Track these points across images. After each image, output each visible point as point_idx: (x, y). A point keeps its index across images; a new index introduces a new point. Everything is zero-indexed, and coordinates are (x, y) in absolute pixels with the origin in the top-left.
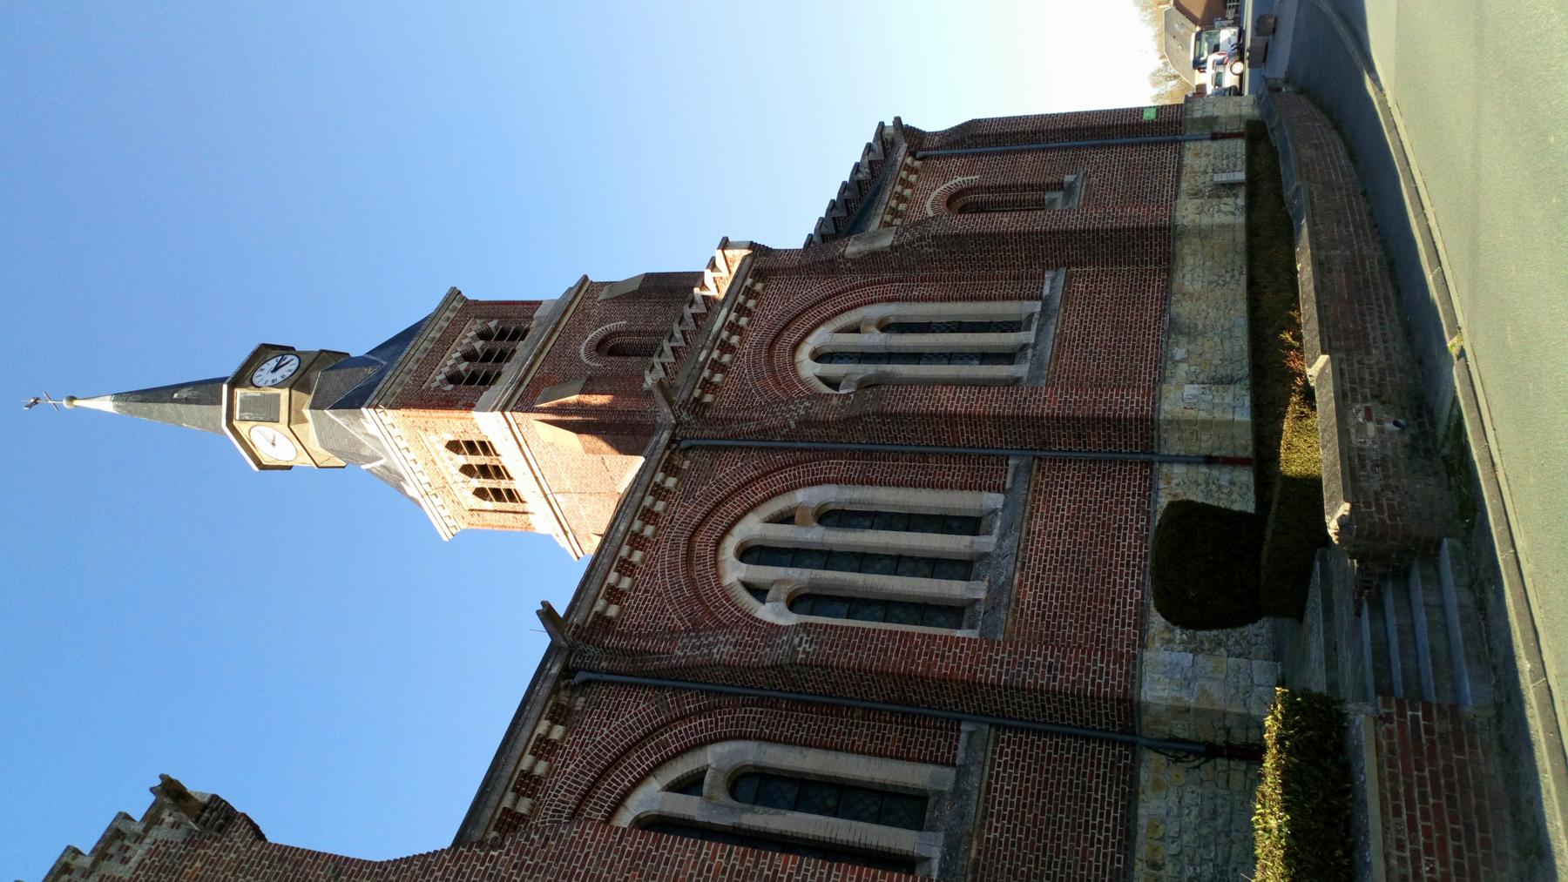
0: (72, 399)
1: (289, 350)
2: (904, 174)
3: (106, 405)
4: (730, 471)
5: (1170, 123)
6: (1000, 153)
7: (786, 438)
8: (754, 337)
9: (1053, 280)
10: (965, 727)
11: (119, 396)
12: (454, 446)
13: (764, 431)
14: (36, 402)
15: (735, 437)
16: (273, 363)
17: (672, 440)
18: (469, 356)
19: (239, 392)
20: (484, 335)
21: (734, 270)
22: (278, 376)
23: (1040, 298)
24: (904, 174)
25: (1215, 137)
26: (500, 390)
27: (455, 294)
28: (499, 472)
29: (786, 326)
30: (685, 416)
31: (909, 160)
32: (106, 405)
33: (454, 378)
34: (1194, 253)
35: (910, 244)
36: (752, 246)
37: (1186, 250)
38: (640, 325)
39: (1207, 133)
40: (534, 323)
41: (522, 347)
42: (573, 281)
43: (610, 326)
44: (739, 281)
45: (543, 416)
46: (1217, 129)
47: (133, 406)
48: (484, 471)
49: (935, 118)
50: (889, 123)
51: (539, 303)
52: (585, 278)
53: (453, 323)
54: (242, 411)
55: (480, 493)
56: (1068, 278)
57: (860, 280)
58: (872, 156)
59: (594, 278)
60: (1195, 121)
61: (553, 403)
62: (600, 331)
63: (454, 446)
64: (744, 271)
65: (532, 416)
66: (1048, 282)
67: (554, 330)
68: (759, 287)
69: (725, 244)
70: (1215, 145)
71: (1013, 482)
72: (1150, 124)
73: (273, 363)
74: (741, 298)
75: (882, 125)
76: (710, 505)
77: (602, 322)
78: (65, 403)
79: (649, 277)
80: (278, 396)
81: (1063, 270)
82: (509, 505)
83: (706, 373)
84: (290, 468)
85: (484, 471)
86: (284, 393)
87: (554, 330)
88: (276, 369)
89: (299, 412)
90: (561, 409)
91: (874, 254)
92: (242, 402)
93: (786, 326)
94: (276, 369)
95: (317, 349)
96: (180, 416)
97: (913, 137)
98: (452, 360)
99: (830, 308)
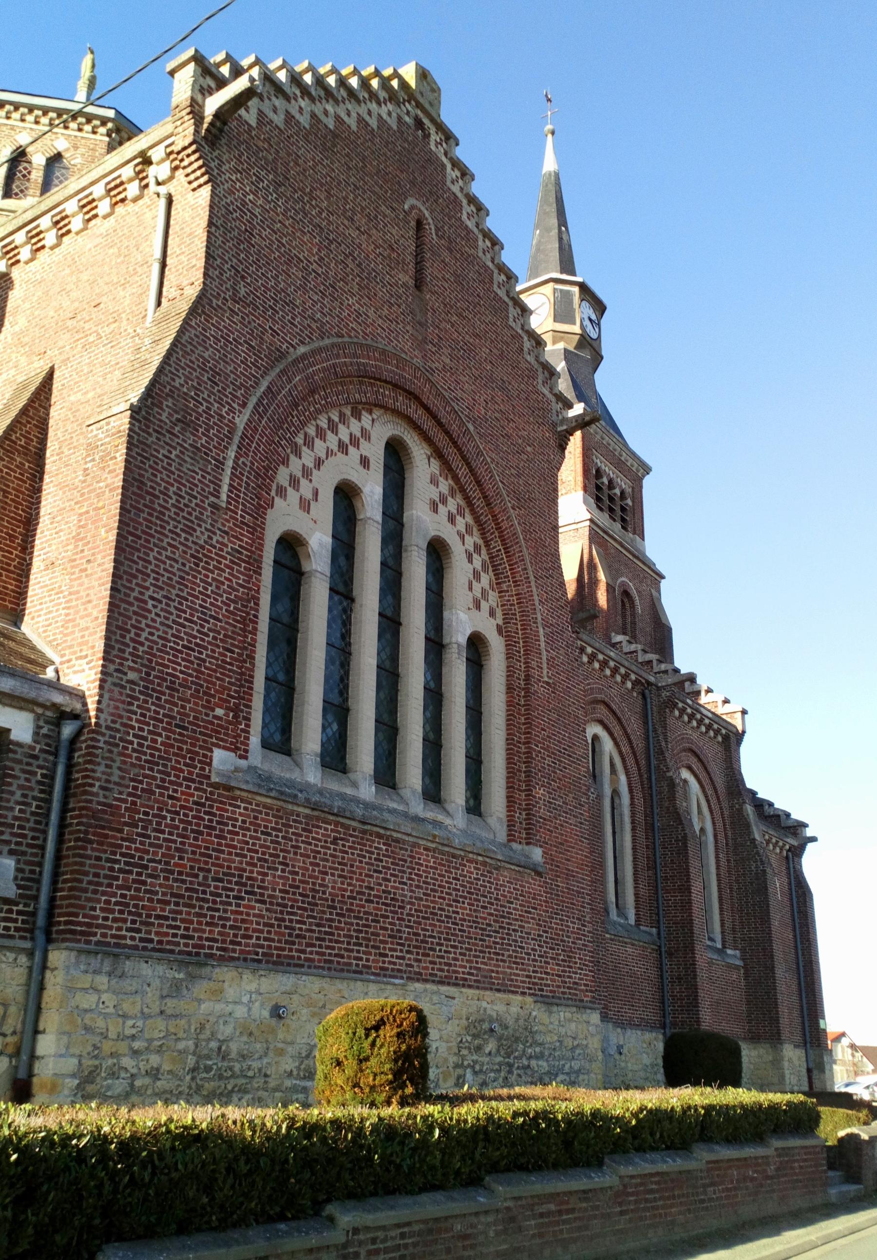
0: (553, 133)
2: (781, 844)
3: (550, 164)
4: (634, 726)
5: (818, 1039)
6: (793, 915)
7: (658, 767)
8: (695, 736)
9: (735, 956)
10: (654, 930)
11: (557, 175)
13: (662, 753)
14: (549, 100)
15: (655, 730)
16: (594, 317)
17: (649, 683)
18: (611, 485)
19: (576, 290)
21: (724, 717)
22: (587, 323)
23: (724, 947)
24: (781, 844)
25: (809, 1071)
26: (604, 519)
27: (647, 470)
29: (700, 760)
30: (665, 694)
31: (787, 847)
32: (550, 164)
33: (599, 474)
34: (760, 1057)
35: (758, 853)
36: (744, 732)
37: (762, 1051)
38: (639, 625)
39: (811, 1065)
40: (631, 535)
41: (618, 526)
42: (660, 567)
43: (637, 601)
44: (724, 724)
45: (586, 552)
46: (815, 1072)
47: (552, 188)
49: (812, 864)
50: (809, 832)
51: (643, 538)
52: (663, 577)
53: (630, 470)
54: (561, 291)
56: (737, 967)
57: (726, 813)
58: (783, 817)
60: (822, 1057)
61: (597, 560)
62: (634, 593)
64: (730, 728)
65: (587, 542)
66: (648, 929)
67: (634, 556)
68: (720, 739)
69: (744, 712)
70: (804, 1071)
71: (646, 932)
72: (818, 1024)
73: (594, 317)
74: (716, 726)
75: (805, 825)
76: (619, 714)
77: (638, 592)
78: (549, 127)
79: (670, 630)
80: (574, 324)
81: (739, 963)
83: (680, 705)
86: (577, 329)
87: (634, 556)
88: (590, 320)
89: (562, 339)
90: (592, 566)
91: (748, 826)
92: (568, 292)
93: (700, 760)
94: (590, 320)
95: (603, 353)
96: (548, 230)
97: (798, 851)
98: (609, 470)
99: (710, 792)
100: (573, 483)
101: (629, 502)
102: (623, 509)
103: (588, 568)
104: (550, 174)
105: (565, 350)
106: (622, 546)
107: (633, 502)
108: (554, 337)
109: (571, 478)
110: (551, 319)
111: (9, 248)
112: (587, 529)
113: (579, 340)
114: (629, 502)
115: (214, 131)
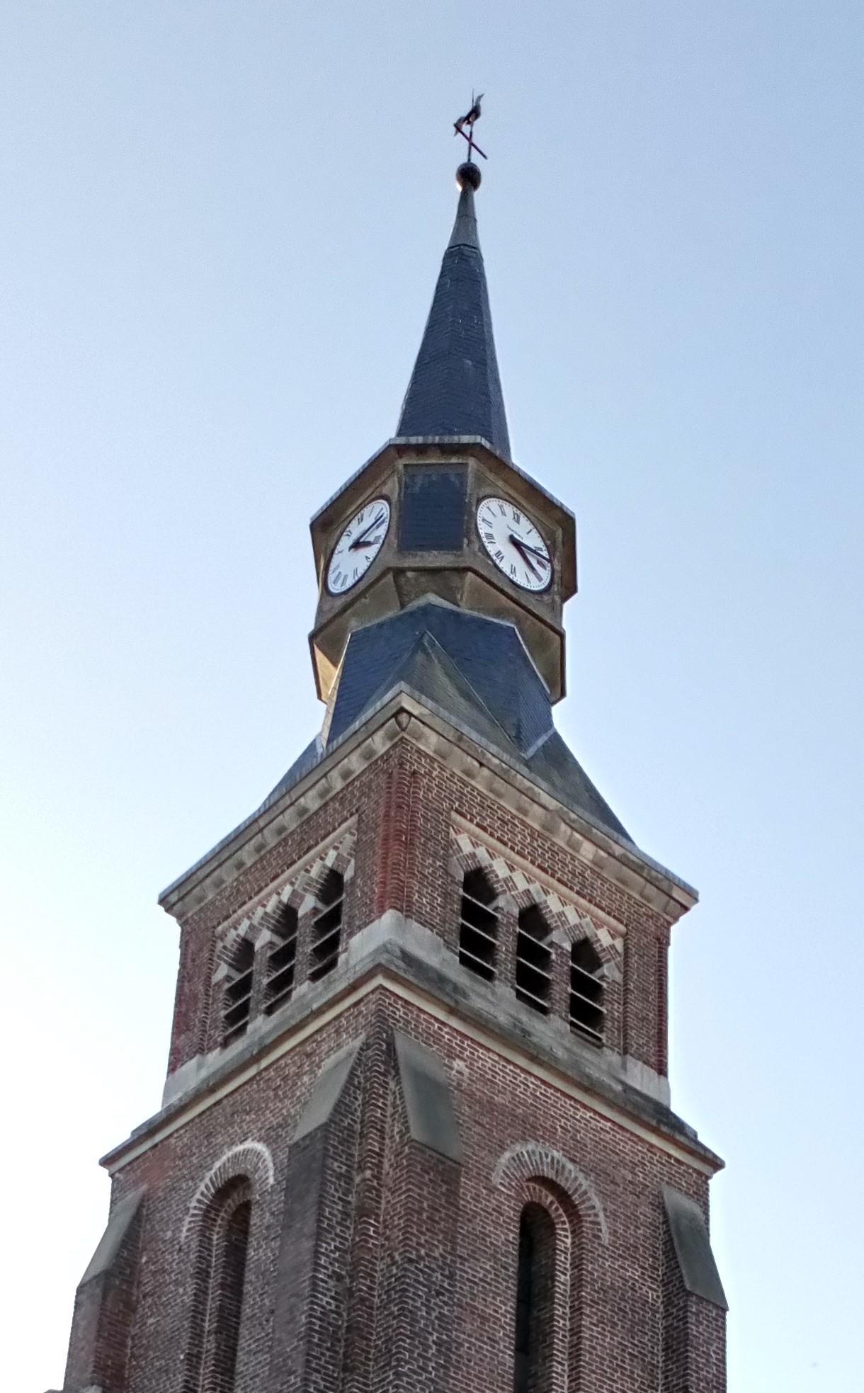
1: (566, 584)
18: (532, 917)
20: (584, 951)
27: (674, 897)
33: (478, 881)
40: (613, 1057)
51: (661, 1069)
59: (717, 1183)
73: (533, 540)
88: (517, 544)
94: (517, 544)
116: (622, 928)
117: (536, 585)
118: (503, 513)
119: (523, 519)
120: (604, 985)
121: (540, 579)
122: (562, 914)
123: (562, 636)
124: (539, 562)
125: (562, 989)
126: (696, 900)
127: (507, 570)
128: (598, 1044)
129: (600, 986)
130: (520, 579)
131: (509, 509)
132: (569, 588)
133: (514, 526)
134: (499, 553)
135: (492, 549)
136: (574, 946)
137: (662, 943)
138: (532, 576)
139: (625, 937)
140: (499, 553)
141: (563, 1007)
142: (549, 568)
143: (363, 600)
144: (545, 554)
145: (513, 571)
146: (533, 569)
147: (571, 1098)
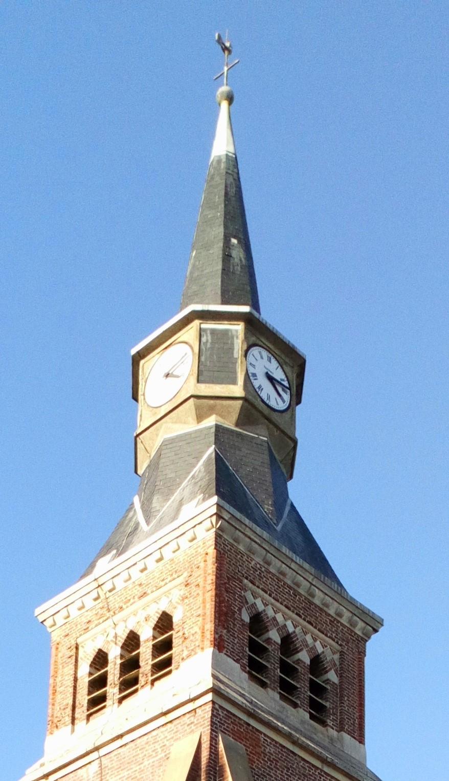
0: (230, 99)
1: (297, 398)
3: (222, 145)
11: (233, 163)
12: (165, 623)
16: (279, 375)
18: (288, 644)
19: (239, 328)
20: (317, 664)
26: (242, 686)
27: (374, 624)
28: (129, 684)
33: (258, 623)
40: (333, 733)
48: (131, 664)
51: (361, 740)
53: (334, 622)
54: (213, 332)
55: (101, 659)
61: (224, 760)
63: (165, 623)
65: (206, 730)
67: (324, 761)
73: (279, 375)
78: (224, 89)
80: (234, 382)
82: (83, 698)
84: (135, 397)
85: (131, 664)
86: (237, 390)
87: (324, 761)
88: (271, 379)
89: (211, 410)
92: (226, 332)
94: (271, 379)
95: (299, 434)
96: (207, 247)
98: (283, 619)
100: (198, 636)
101: (332, 676)
102: (317, 689)
103: (208, 773)
104: (219, 161)
105: (218, 428)
106: (295, 742)
107: (341, 676)
108: (198, 408)
109: (196, 629)
110: (193, 379)
111: (227, 717)
112: (209, 707)
113: (242, 408)
114: (332, 676)
115: (218, 575)
116: (339, 648)
117: (282, 406)
118: (262, 358)
119: (273, 360)
120: (328, 687)
121: (284, 401)
122: (274, 619)
123: (295, 442)
124: (283, 390)
125: (305, 691)
126: (382, 625)
127: (265, 398)
128: (323, 723)
129: (326, 689)
130: (272, 403)
131: (265, 354)
132: (299, 402)
133: (268, 364)
134: (260, 387)
135: (256, 384)
136: (282, 640)
137: (362, 654)
138: (279, 399)
139: (342, 653)
140: (260, 387)
141: (307, 701)
142: (289, 393)
143: (275, 430)
144: (286, 383)
145: (269, 398)
146: (279, 395)
147: (308, 762)
